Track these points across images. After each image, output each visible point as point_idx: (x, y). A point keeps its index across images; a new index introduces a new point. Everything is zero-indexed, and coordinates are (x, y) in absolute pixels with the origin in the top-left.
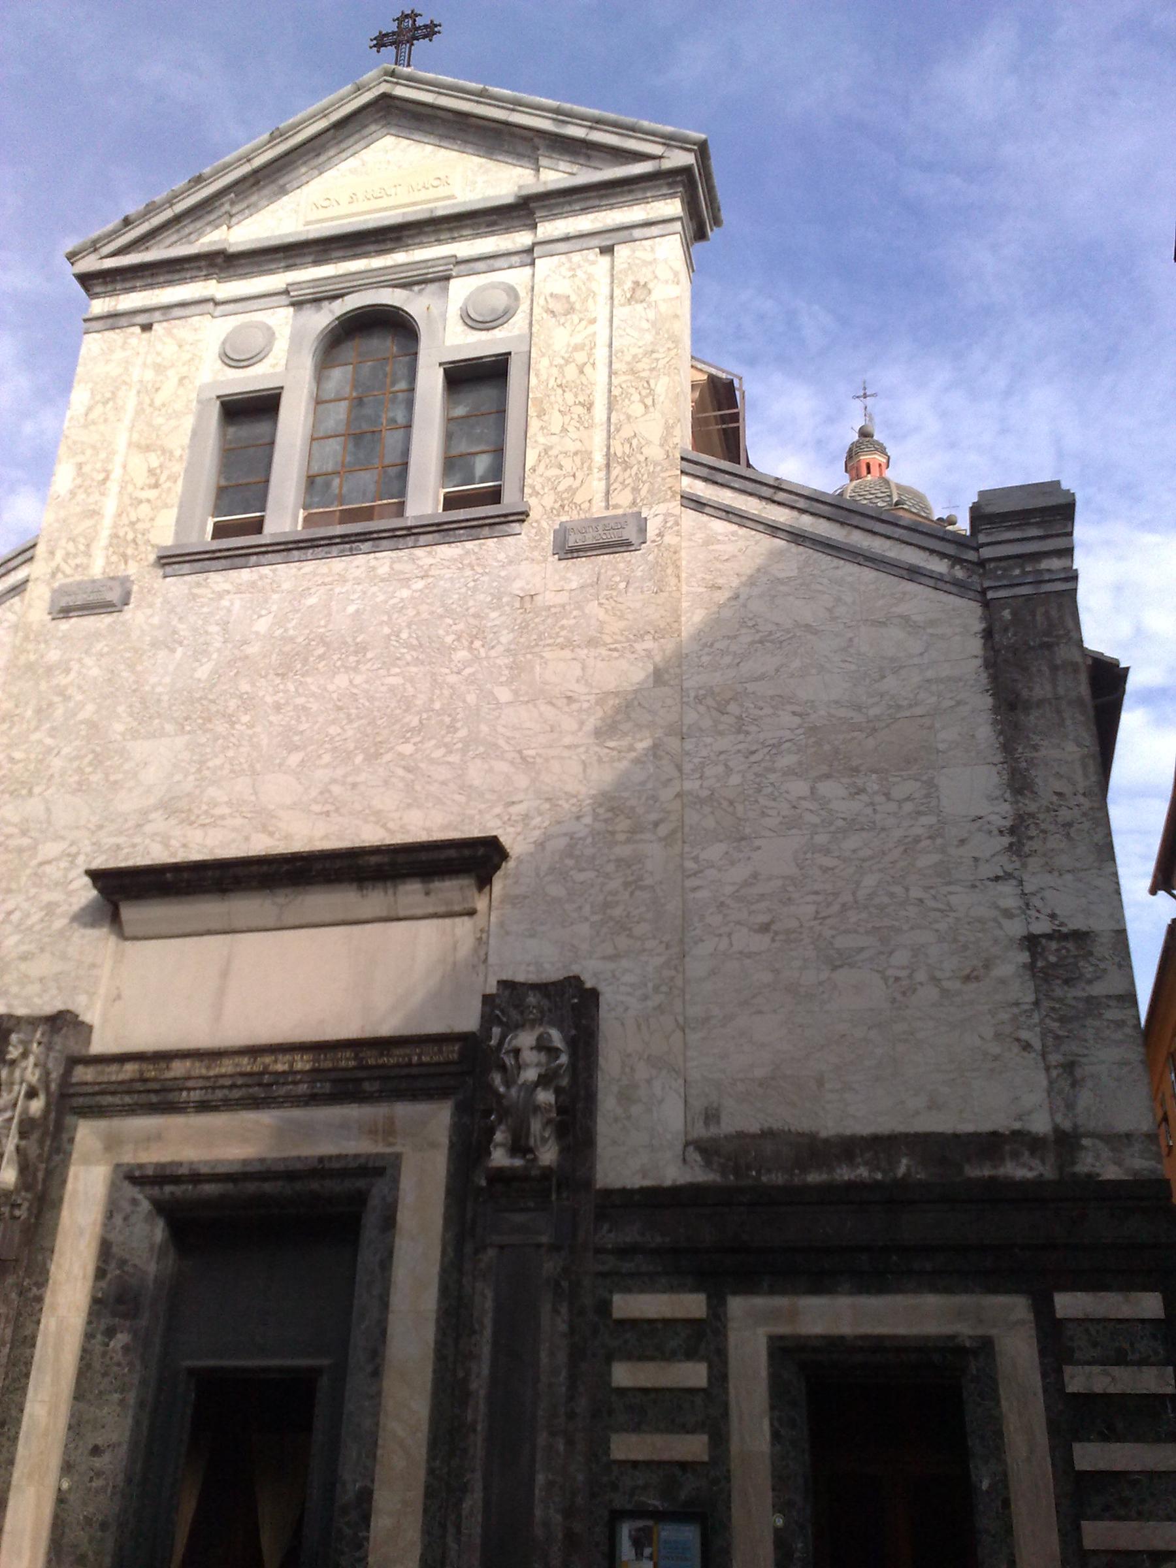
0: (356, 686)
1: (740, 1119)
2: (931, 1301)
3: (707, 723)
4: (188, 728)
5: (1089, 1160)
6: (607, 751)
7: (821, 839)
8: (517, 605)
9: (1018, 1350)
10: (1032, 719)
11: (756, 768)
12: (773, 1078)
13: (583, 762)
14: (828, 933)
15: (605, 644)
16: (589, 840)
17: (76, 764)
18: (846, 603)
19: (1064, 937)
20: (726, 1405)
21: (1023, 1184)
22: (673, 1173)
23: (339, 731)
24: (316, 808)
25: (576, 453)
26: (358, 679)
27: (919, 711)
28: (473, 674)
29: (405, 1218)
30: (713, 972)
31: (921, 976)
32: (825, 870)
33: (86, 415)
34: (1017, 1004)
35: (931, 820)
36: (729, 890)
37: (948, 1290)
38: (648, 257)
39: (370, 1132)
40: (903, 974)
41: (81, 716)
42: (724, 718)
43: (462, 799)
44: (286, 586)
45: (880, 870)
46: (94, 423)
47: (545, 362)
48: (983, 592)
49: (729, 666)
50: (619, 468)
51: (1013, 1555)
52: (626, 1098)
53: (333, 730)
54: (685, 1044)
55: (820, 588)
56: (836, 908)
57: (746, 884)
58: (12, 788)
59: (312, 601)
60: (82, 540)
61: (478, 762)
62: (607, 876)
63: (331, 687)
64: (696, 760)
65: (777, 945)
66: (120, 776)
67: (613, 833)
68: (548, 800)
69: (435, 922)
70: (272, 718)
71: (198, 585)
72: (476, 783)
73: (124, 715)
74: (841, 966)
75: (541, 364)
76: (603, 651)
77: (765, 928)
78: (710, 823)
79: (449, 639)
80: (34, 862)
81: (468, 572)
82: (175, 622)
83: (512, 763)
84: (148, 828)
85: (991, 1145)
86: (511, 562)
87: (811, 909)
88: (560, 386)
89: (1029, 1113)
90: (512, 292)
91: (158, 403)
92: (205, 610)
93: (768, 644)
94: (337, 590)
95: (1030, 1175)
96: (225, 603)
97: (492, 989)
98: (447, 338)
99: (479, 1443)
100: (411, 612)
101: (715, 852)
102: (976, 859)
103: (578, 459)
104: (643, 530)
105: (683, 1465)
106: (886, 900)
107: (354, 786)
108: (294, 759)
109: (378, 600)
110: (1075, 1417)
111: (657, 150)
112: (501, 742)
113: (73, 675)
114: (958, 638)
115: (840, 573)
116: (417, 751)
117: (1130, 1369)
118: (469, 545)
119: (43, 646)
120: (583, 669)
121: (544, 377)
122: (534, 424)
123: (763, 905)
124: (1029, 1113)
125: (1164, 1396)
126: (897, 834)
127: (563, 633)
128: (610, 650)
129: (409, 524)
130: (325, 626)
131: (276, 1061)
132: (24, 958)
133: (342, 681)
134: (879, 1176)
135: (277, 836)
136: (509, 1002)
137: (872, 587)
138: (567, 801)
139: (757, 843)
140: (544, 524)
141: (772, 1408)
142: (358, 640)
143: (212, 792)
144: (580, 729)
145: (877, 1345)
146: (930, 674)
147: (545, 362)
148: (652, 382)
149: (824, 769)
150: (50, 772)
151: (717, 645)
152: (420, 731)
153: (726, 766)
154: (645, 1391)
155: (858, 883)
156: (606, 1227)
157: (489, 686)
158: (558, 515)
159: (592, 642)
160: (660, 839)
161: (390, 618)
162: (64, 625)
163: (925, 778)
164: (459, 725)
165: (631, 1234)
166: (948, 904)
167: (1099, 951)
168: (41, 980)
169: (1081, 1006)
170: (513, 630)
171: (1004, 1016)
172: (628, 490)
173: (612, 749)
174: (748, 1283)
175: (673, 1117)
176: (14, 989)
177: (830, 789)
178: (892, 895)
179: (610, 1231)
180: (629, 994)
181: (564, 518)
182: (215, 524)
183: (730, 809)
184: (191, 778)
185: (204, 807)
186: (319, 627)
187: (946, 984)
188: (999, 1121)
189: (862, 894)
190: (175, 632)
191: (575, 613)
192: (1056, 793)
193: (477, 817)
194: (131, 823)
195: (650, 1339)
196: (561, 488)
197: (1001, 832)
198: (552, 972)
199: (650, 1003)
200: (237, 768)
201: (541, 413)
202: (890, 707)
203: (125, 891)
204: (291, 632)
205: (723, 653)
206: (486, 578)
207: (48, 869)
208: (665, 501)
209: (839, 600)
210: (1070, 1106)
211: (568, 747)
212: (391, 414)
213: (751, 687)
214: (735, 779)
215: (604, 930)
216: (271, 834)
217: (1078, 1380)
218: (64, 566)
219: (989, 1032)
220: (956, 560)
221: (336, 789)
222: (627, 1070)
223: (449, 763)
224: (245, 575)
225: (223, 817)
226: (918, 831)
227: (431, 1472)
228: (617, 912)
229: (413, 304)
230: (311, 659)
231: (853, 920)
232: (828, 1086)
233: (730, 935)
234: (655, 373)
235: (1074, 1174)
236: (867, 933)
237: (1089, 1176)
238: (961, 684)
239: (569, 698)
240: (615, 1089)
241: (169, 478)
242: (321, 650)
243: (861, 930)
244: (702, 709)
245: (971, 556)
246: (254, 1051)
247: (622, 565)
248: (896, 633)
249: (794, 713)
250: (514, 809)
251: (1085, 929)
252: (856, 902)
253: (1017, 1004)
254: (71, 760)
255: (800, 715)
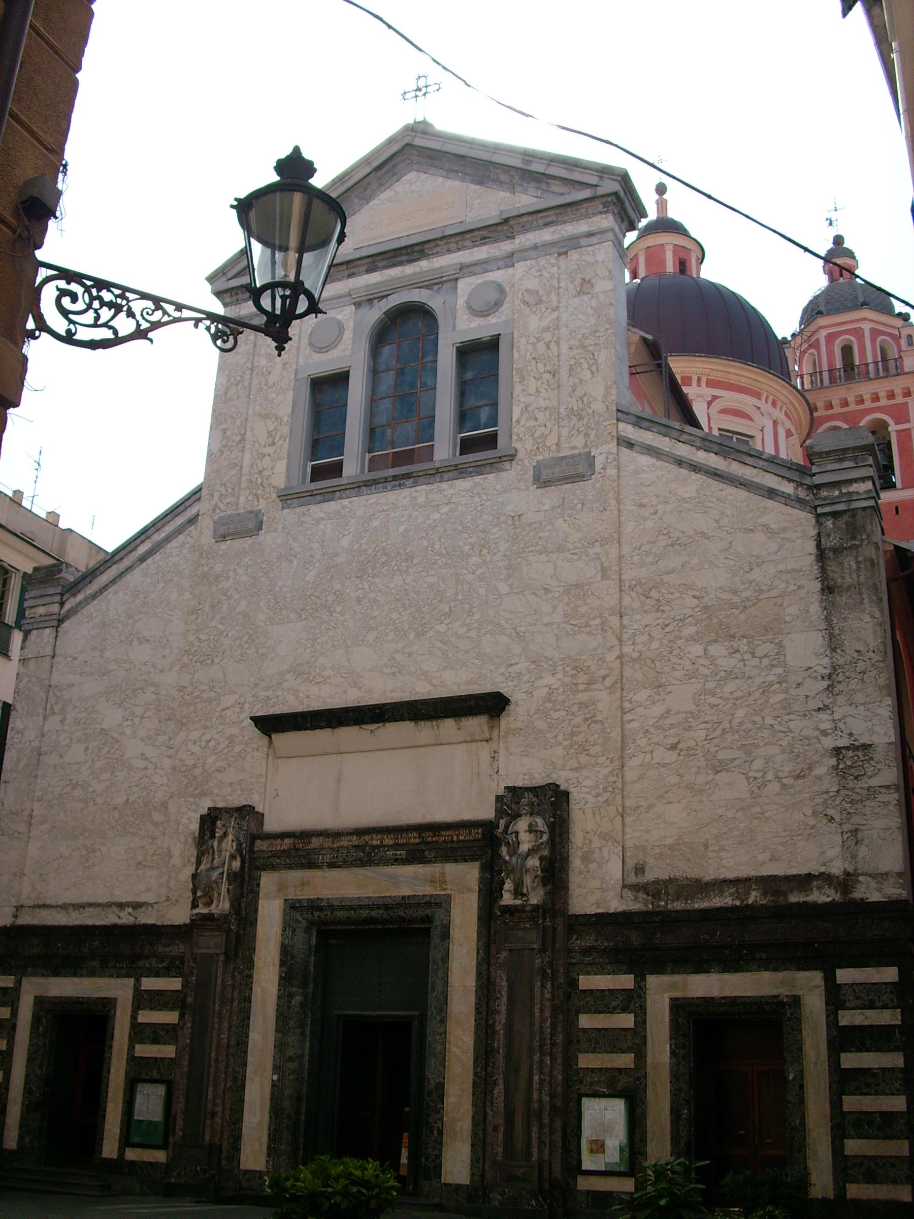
0: (407, 584)
1: (656, 872)
2: (766, 976)
3: (636, 605)
4: (304, 616)
5: (863, 890)
6: (571, 627)
7: (711, 685)
8: (510, 522)
9: (814, 1003)
10: (842, 599)
11: (669, 637)
12: (677, 844)
13: (556, 635)
14: (713, 749)
15: (569, 550)
16: (561, 689)
17: (238, 642)
18: (727, 516)
19: (857, 748)
20: (645, 1038)
21: (825, 904)
22: (615, 905)
23: (398, 616)
24: (387, 670)
25: (546, 409)
26: (409, 580)
27: (774, 593)
28: (483, 573)
29: (456, 933)
30: (641, 777)
31: (770, 776)
32: (713, 706)
33: (226, 394)
34: (827, 792)
35: (780, 670)
36: (651, 721)
37: (775, 970)
38: (590, 259)
39: (431, 882)
40: (758, 775)
41: (238, 610)
42: (648, 601)
43: (479, 663)
44: (360, 513)
45: (747, 706)
46: (231, 399)
47: (523, 341)
48: (815, 508)
49: (651, 563)
50: (575, 419)
51: (804, 1115)
52: (586, 859)
53: (394, 616)
54: (623, 824)
55: (710, 505)
56: (718, 732)
57: (662, 717)
58: (202, 659)
59: (376, 523)
60: (230, 485)
61: (488, 636)
62: (573, 714)
63: (392, 585)
64: (630, 631)
65: (682, 757)
66: (265, 650)
67: (576, 684)
68: (534, 662)
69: (465, 745)
70: (355, 608)
71: (304, 514)
72: (488, 651)
73: (265, 608)
74: (721, 771)
75: (521, 343)
76: (569, 556)
77: (674, 747)
78: (639, 676)
79: (466, 548)
80: (219, 709)
81: (477, 499)
82: (291, 541)
83: (510, 636)
84: (286, 685)
85: (805, 881)
86: (505, 491)
87: (704, 733)
88: (534, 358)
89: (831, 861)
90: (500, 289)
91: (270, 382)
92: (310, 532)
93: (677, 547)
94: (393, 515)
95: (828, 900)
96: (321, 527)
97: (501, 792)
98: (459, 325)
99: (501, 1060)
100: (441, 530)
101: (642, 696)
102: (807, 697)
103: (547, 413)
104: (592, 465)
105: (620, 1070)
106: (750, 726)
107: (410, 654)
108: (371, 636)
109: (419, 521)
110: (843, 1039)
111: (593, 180)
112: (503, 622)
113: (231, 581)
114: (799, 541)
115: (723, 494)
116: (448, 629)
117: (876, 1011)
118: (478, 479)
119: (211, 560)
120: (555, 568)
121: (523, 352)
122: (518, 388)
123: (673, 731)
124: (831, 861)
125: (894, 1026)
126: (758, 681)
127: (541, 543)
128: (573, 554)
129: (437, 465)
130: (386, 542)
131: (372, 839)
132: (219, 771)
133: (398, 580)
134: (738, 903)
135: (363, 689)
136: (512, 800)
137: (745, 504)
138: (546, 663)
139: (669, 689)
140: (526, 462)
141: (671, 1038)
142: (407, 551)
143: (322, 660)
144: (554, 612)
145: (734, 1001)
146: (781, 567)
147: (523, 341)
148: (596, 354)
149: (713, 636)
150: (224, 647)
151: (643, 548)
152: (450, 615)
153: (650, 635)
154: (599, 1030)
155: (733, 715)
156: (575, 937)
157: (493, 582)
158: (535, 455)
159: (560, 549)
160: (607, 689)
161: (427, 534)
162: (224, 546)
163: (776, 641)
164: (474, 610)
165: (589, 941)
166: (788, 728)
167: (878, 756)
168: (231, 784)
169: (865, 792)
170: (508, 541)
171: (819, 800)
172: (582, 435)
173: (575, 625)
174: (659, 969)
175: (614, 870)
176: (216, 790)
177: (716, 650)
178: (754, 723)
179: (577, 939)
180: (587, 793)
181: (540, 458)
182: (313, 467)
183: (653, 666)
184: (308, 651)
185: (318, 671)
186: (382, 542)
187: (785, 781)
188: (814, 868)
189: (735, 722)
190: (291, 549)
191: (549, 527)
192: (857, 651)
193: (489, 675)
194: (274, 682)
195: (603, 1001)
196: (537, 435)
197: (823, 678)
198: (539, 780)
199: (601, 799)
200: (336, 643)
201: (522, 379)
202: (756, 591)
203: (270, 725)
204: (364, 547)
205: (647, 553)
206: (489, 503)
207: (228, 713)
208: (606, 443)
209: (723, 513)
210: (854, 856)
211: (546, 625)
212: (423, 380)
213: (666, 578)
214: (655, 645)
215: (572, 751)
216: (360, 689)
217: (846, 1018)
218: (220, 504)
219: (809, 813)
220: (800, 484)
221: (399, 657)
222: (587, 842)
223: (469, 637)
224: (332, 506)
225: (329, 677)
226: (772, 678)
227: (475, 1074)
228: (579, 739)
229: (434, 301)
230: (378, 565)
231: (729, 740)
232: (710, 848)
233: (652, 752)
234: (598, 347)
235: (852, 899)
236: (738, 748)
237: (862, 900)
238: (801, 574)
239: (546, 589)
240: (580, 854)
241: (281, 437)
242: (384, 559)
243: (734, 746)
244: (633, 594)
245: (808, 481)
246: (360, 832)
247: (578, 492)
248: (760, 537)
249: (694, 597)
250: (512, 669)
251: (869, 743)
252: (731, 728)
253: (827, 792)
254: (235, 640)
255: (698, 598)
